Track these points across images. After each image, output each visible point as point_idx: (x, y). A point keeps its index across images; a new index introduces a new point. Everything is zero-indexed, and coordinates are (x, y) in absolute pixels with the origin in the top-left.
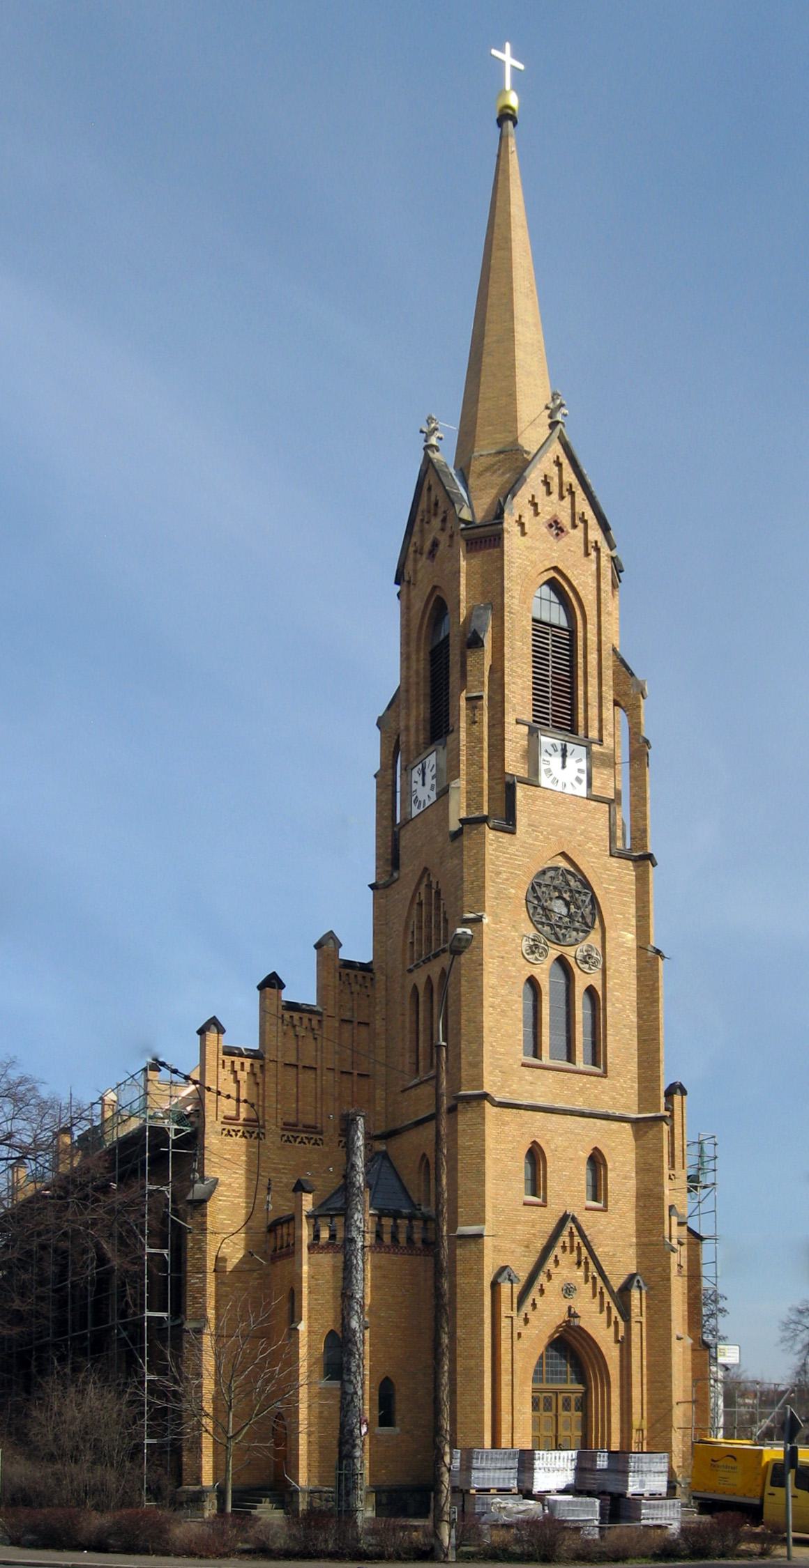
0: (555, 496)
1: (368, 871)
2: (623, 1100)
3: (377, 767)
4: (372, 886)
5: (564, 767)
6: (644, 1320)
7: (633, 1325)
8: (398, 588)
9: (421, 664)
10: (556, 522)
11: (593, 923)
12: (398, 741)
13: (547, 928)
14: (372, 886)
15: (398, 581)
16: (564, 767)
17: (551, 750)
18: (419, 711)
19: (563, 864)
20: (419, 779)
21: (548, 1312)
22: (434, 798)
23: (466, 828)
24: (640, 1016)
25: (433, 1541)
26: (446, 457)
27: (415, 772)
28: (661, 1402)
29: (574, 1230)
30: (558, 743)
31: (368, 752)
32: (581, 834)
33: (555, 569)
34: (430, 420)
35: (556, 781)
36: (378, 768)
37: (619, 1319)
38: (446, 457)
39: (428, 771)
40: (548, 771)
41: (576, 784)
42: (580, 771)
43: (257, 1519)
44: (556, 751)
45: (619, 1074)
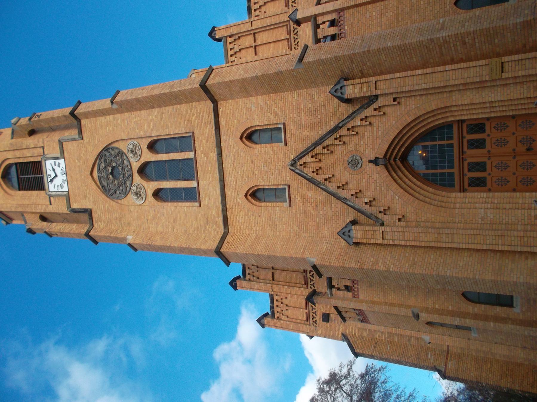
2: (206, 116)
6: (373, 79)
7: (379, 92)
11: (117, 148)
13: (128, 183)
19: (96, 174)
21: (375, 183)
24: (153, 107)
28: (464, 43)
29: (302, 162)
32: (80, 162)
37: (375, 106)
45: (190, 121)
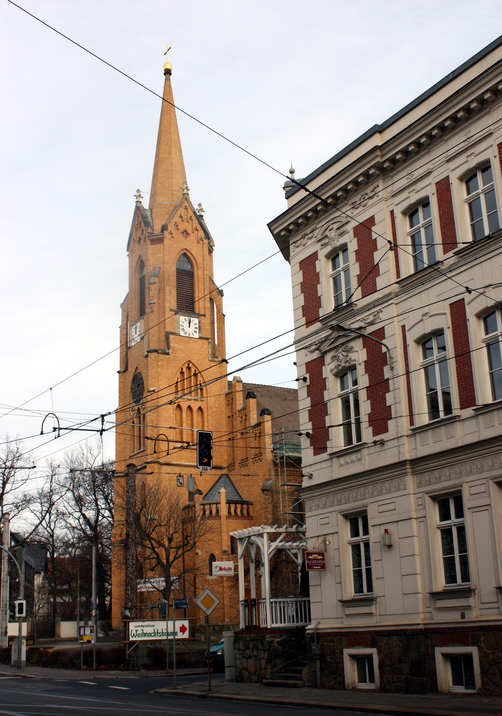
0: (185, 221)
1: (117, 367)
3: (120, 323)
4: (119, 372)
5: (189, 327)
8: (128, 253)
9: (138, 282)
10: (185, 231)
12: (128, 314)
14: (119, 372)
15: (128, 250)
16: (189, 327)
17: (184, 321)
18: (136, 303)
20: (134, 331)
22: (139, 340)
23: (149, 354)
25: (225, 579)
26: (146, 204)
27: (133, 327)
30: (187, 318)
31: (116, 319)
33: (186, 249)
34: (138, 191)
35: (186, 333)
36: (380, 124)
38: (146, 204)
39: (137, 328)
40: (183, 329)
41: (194, 333)
42: (196, 328)
43: (160, 576)
44: (186, 321)
